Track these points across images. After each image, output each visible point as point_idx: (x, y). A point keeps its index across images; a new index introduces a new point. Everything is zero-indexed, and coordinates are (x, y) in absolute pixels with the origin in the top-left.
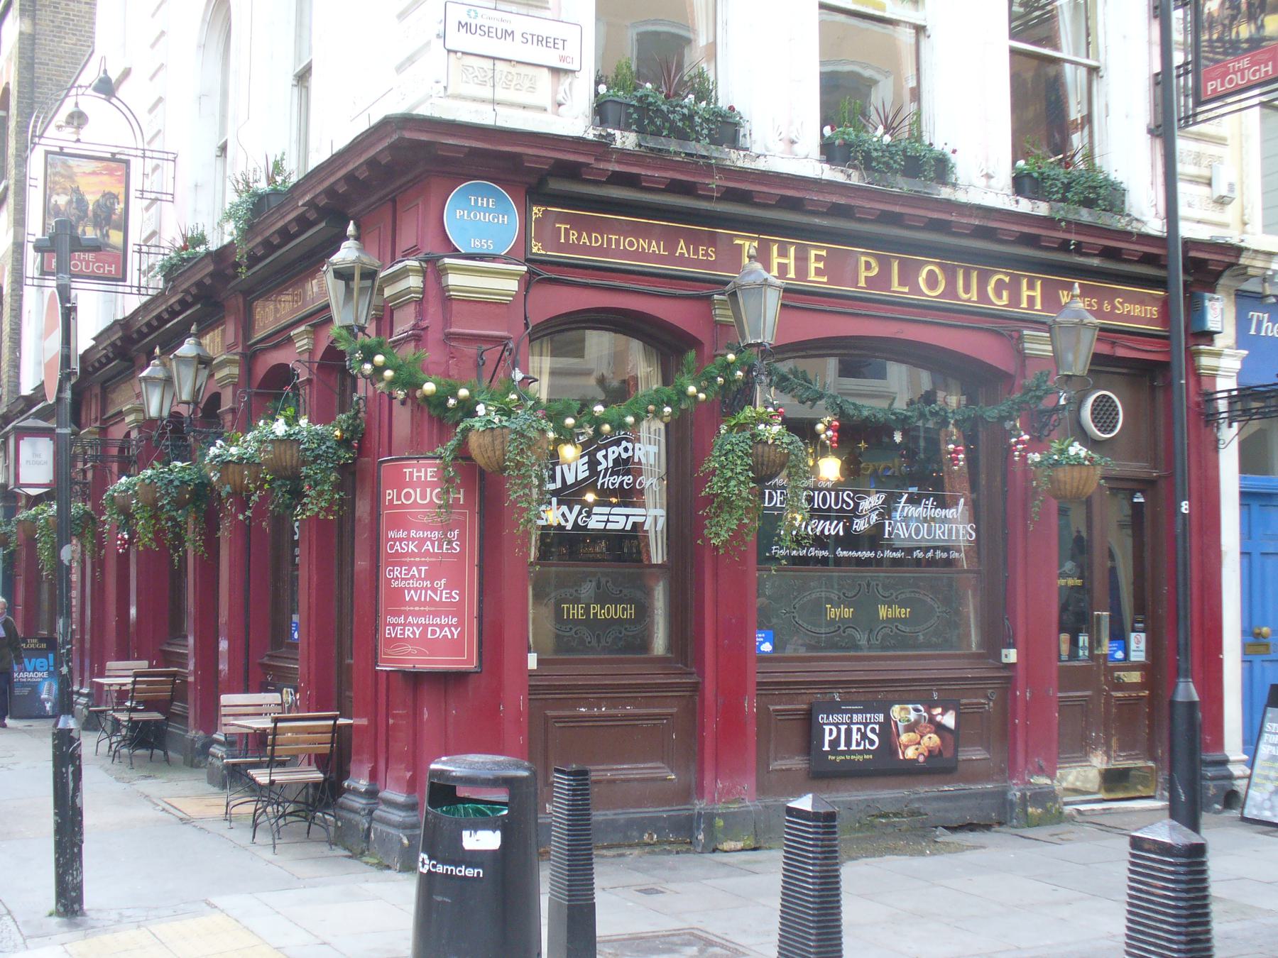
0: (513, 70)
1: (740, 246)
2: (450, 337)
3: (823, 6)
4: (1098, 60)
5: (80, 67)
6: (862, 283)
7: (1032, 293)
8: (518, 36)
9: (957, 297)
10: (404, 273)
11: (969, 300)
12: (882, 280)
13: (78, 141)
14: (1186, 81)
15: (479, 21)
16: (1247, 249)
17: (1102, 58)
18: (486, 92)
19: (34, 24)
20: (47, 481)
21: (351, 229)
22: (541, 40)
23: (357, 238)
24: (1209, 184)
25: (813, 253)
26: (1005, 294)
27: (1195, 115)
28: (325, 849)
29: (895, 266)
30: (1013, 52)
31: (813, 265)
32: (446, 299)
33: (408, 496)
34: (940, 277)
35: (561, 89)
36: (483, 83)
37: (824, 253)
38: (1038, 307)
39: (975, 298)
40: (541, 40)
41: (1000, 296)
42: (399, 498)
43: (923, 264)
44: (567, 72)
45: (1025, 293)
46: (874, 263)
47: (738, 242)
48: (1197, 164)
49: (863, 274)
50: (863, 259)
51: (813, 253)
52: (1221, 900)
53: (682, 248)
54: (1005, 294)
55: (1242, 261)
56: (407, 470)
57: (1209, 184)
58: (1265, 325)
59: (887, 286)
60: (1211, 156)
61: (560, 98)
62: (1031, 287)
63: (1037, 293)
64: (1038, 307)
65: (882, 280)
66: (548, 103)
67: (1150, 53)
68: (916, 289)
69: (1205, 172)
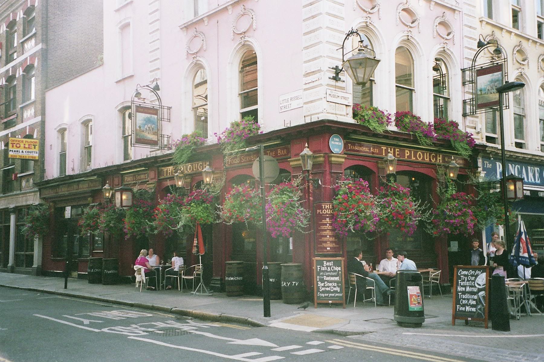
0: (339, 106)
1: (382, 149)
3: (514, 114)
4: (414, 87)
5: (83, 73)
6: (406, 157)
7: (440, 158)
8: (340, 97)
9: (425, 160)
10: (320, 157)
11: (427, 161)
12: (410, 157)
13: (145, 103)
14: (473, 103)
15: (333, 94)
16: (488, 146)
17: (450, 96)
18: (334, 112)
19: (47, 46)
20: (130, 205)
21: (306, 145)
22: (344, 98)
23: (308, 147)
24: (475, 129)
26: (434, 159)
27: (476, 112)
28: (35, 276)
29: (413, 152)
30: (434, 95)
31: (397, 153)
32: (330, 163)
33: (325, 212)
34: (421, 155)
35: (348, 110)
36: (334, 109)
37: (399, 150)
38: (441, 162)
39: (428, 160)
40: (344, 98)
41: (433, 160)
42: (322, 212)
43: (418, 151)
44: (349, 106)
45: (438, 158)
46: (408, 152)
47: (382, 148)
48: (473, 123)
49: (406, 155)
50: (406, 151)
51: (397, 150)
52: (62, 288)
54: (434, 159)
55: (487, 149)
56: (323, 205)
57: (475, 129)
58: (488, 164)
60: (475, 121)
61: (348, 112)
63: (441, 158)
64: (441, 162)
66: (345, 114)
67: (182, 25)
68: (417, 159)
69: (474, 126)
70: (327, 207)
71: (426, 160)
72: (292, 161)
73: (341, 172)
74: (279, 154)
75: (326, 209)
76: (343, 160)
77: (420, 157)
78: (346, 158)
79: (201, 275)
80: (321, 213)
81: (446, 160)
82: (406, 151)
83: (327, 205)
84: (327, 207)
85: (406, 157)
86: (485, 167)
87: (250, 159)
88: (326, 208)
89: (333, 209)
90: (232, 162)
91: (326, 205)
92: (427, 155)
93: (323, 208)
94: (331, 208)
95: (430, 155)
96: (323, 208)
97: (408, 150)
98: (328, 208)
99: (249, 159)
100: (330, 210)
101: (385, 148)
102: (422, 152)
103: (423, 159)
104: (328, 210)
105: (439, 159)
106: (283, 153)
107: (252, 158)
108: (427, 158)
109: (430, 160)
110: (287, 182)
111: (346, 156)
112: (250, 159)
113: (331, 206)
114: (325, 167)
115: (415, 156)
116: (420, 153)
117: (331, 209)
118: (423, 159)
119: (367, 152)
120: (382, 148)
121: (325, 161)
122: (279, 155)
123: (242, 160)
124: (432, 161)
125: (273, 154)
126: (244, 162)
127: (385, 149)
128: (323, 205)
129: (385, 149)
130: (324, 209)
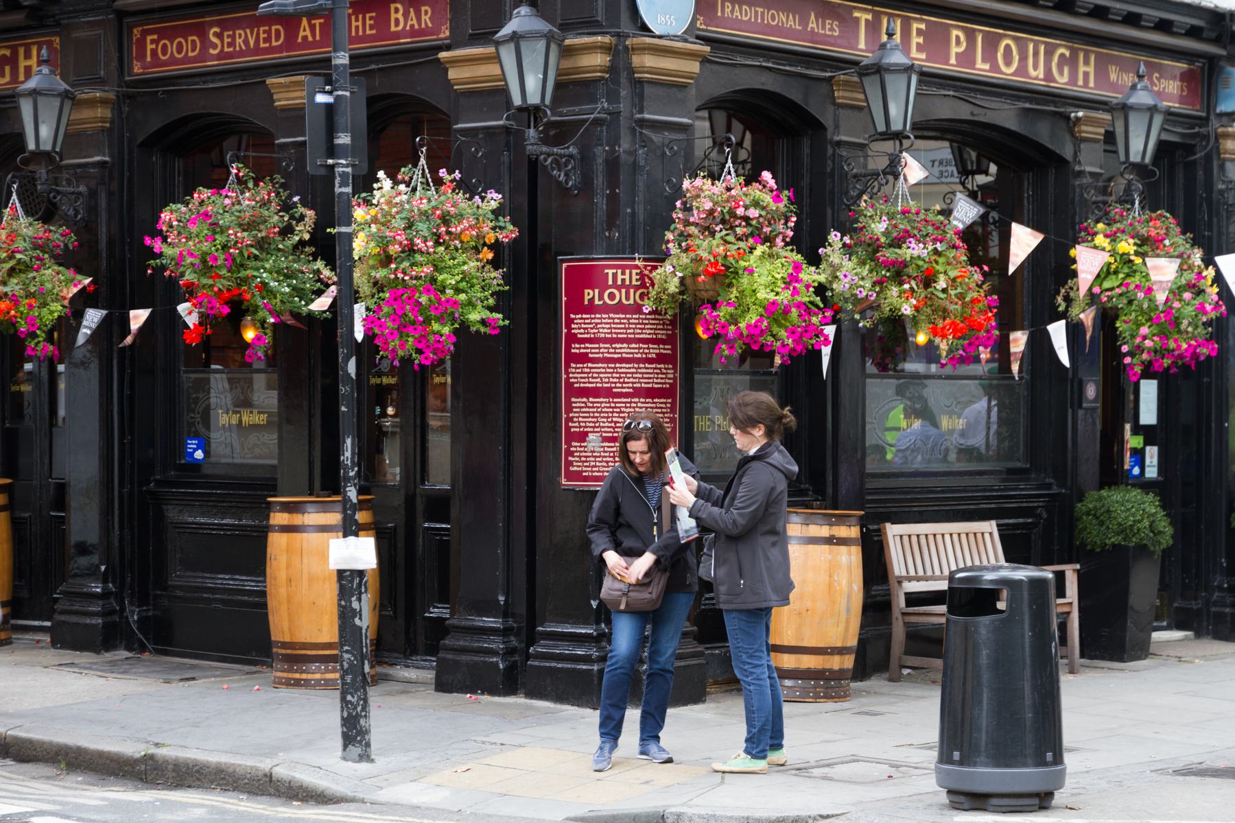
1: (858, 19)
2: (642, 123)
6: (953, 61)
11: (1036, 78)
25: (915, 26)
26: (1066, 70)
37: (923, 26)
38: (1092, 84)
39: (1041, 76)
42: (601, 298)
43: (1059, 46)
45: (1082, 68)
47: (856, 14)
49: (955, 50)
50: (955, 33)
51: (915, 26)
53: (304, 30)
54: (1066, 70)
56: (610, 272)
59: (972, 64)
62: (1086, 63)
63: (1091, 69)
64: (1092, 84)
65: (967, 58)
70: (623, 280)
71: (1032, 73)
72: (456, 62)
73: (861, 141)
74: (397, 24)
75: (619, 288)
76: (694, 67)
77: (1008, 61)
78: (705, 61)
79: (785, 504)
80: (597, 302)
81: (1113, 77)
82: (955, 33)
83: (623, 273)
84: (623, 280)
85: (953, 61)
86: (719, 14)
87: (252, 43)
88: (619, 283)
89: (643, 286)
90: (164, 54)
91: (619, 271)
92: (1036, 54)
93: (610, 282)
94: (634, 283)
95: (1049, 53)
96: (610, 282)
97: (962, 28)
98: (627, 283)
99: (246, 42)
100: (632, 291)
101: (869, 17)
102: (1015, 39)
103: (1022, 70)
104: (623, 291)
105: (1086, 75)
106: (415, 22)
107: (262, 36)
108: (1036, 67)
109: (1049, 76)
110: (865, 201)
111: (708, 49)
112: (252, 43)
113: (634, 277)
114: (613, 97)
115: (990, 56)
116: (1009, 42)
117: (637, 288)
118: (1022, 70)
119: (789, 33)
120: (856, 14)
121: (612, 69)
122: (393, 28)
123: (215, 46)
124: (1055, 81)
125: (368, 22)
126: (222, 56)
127: (867, 20)
128: (610, 272)
129: (867, 20)
130: (610, 287)
